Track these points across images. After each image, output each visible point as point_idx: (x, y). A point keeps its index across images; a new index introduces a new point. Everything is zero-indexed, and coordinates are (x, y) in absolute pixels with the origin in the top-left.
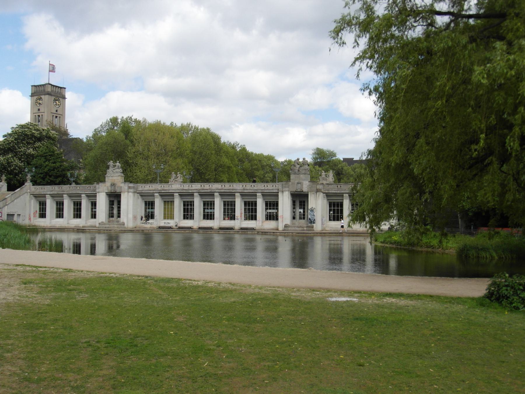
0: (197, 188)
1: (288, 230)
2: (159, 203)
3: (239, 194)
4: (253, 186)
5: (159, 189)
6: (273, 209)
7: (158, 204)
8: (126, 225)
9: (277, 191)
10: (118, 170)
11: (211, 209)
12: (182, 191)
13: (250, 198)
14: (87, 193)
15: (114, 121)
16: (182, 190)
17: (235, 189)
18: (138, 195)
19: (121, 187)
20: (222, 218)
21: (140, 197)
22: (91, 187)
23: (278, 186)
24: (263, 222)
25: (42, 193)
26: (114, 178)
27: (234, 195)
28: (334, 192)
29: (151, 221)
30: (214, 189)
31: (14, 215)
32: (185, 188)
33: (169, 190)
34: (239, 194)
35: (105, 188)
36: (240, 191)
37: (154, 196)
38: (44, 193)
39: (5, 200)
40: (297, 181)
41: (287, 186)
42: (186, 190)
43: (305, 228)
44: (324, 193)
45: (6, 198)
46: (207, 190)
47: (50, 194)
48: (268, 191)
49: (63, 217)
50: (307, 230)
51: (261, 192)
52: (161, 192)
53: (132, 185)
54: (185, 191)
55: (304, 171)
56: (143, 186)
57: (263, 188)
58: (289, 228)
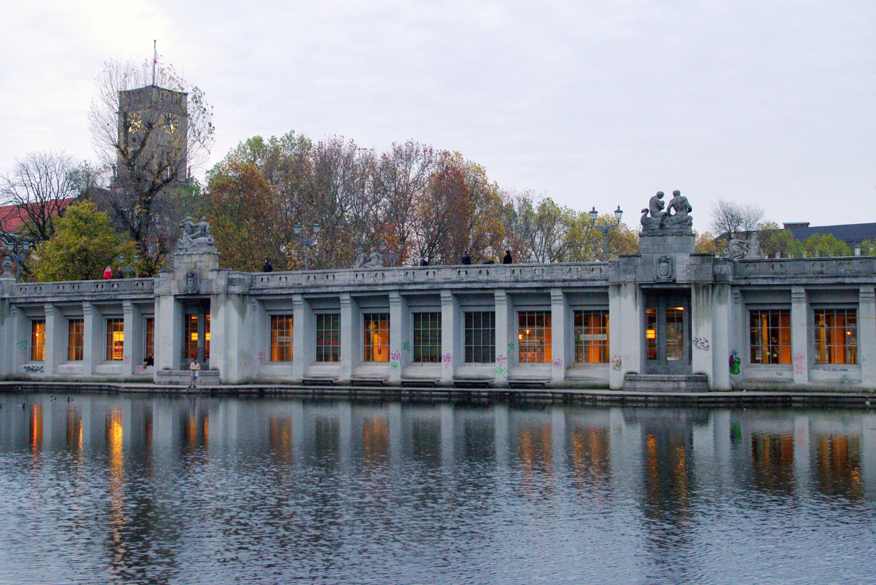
0: (396, 280)
1: (635, 389)
2: (301, 319)
3: (502, 293)
4: (265, 280)
5: (304, 284)
6: (596, 332)
8: (222, 376)
9: (604, 283)
12: (359, 289)
13: (533, 303)
14: (135, 297)
15: (256, 143)
16: (360, 285)
17: (491, 282)
18: (254, 300)
19: (211, 281)
20: (362, 357)
21: (257, 304)
22: (145, 283)
23: (607, 271)
24: (568, 368)
25: (36, 300)
26: (195, 258)
27: (492, 296)
28: (765, 282)
30: (439, 280)
32: (366, 281)
33: (328, 286)
34: (502, 293)
35: (174, 284)
36: (508, 285)
37: (290, 301)
38: (40, 300)
40: (657, 257)
41: (631, 268)
42: (368, 285)
43: (683, 385)
44: (733, 286)
46: (423, 283)
47: (53, 302)
48: (579, 284)
49: (82, 359)
50: (686, 390)
52: (307, 291)
54: (365, 288)
55: (677, 226)
56: (265, 278)
57: (568, 277)
58: (638, 385)
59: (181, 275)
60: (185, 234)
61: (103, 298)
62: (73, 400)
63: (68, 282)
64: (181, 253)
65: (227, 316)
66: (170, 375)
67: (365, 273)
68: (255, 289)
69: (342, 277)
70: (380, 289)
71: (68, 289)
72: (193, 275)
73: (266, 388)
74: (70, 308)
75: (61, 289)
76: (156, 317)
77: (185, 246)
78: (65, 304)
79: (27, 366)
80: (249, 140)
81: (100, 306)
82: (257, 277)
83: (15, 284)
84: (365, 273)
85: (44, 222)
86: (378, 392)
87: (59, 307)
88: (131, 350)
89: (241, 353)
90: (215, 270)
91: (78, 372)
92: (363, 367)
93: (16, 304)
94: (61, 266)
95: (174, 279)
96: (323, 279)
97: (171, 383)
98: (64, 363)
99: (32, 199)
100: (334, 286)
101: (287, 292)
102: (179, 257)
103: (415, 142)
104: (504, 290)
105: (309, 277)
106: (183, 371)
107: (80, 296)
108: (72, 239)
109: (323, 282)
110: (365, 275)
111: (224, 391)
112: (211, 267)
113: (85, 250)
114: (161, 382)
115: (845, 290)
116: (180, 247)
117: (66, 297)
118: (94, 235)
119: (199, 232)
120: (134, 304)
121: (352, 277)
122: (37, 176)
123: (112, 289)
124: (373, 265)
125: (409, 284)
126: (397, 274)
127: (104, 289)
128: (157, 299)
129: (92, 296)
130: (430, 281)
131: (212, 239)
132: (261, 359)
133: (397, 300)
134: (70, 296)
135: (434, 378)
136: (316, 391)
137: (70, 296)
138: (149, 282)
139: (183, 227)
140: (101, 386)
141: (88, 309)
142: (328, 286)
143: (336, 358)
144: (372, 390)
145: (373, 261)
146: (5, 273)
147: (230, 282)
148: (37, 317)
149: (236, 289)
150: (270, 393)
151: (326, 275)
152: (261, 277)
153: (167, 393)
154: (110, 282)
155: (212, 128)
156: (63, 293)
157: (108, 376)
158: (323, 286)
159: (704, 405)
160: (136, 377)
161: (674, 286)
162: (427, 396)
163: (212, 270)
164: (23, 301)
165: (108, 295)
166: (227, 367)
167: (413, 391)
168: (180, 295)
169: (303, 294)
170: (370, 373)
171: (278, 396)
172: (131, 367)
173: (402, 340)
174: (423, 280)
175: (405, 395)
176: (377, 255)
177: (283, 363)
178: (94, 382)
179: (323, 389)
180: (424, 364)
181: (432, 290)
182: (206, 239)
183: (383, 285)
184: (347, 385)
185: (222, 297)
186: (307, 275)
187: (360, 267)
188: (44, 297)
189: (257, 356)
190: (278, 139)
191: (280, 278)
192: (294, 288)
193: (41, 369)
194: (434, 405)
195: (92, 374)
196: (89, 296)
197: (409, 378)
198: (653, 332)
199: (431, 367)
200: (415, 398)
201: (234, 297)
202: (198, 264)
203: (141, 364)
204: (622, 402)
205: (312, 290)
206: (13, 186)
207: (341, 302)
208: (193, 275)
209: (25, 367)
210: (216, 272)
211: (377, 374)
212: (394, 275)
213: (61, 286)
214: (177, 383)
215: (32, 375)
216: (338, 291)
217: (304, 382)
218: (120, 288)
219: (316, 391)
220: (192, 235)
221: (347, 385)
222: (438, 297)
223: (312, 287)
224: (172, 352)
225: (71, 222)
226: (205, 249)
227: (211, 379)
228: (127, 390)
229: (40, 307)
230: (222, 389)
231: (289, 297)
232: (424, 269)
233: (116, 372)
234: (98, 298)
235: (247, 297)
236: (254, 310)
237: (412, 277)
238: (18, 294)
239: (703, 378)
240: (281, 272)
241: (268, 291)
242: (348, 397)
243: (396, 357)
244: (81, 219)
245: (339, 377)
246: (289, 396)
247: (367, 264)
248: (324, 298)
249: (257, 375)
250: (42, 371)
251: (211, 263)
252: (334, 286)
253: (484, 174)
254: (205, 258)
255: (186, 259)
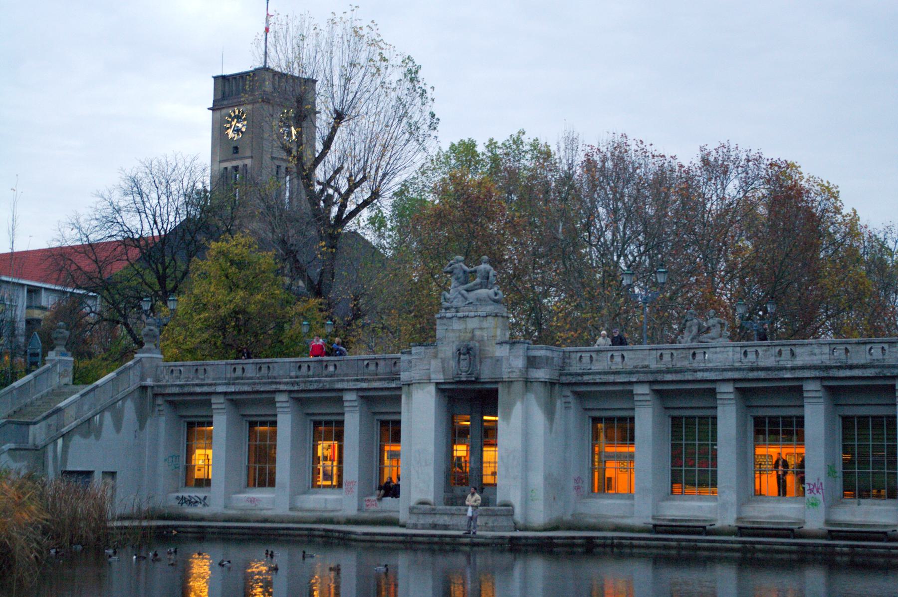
0: (816, 360)
5: (654, 366)
7: (649, 431)
10: (483, 292)
11: (873, 438)
12: (752, 375)
14: (365, 385)
16: (752, 369)
18: (567, 392)
19: (498, 360)
21: (571, 399)
22: (381, 363)
25: (198, 390)
26: (472, 324)
29: (388, 499)
31: (89, 474)
32: (762, 364)
33: (695, 371)
35: (435, 364)
38: (205, 389)
39: (55, 417)
45: (60, 410)
46: (864, 367)
47: (225, 393)
51: (651, 383)
52: (660, 377)
53: (802, 351)
54: (762, 375)
59: (447, 350)
60: (454, 283)
61: (311, 388)
62: (312, 557)
63: (251, 361)
64: (449, 315)
65: (527, 418)
66: (433, 512)
67: (760, 350)
68: (570, 374)
69: (719, 356)
70: (788, 375)
71: (251, 371)
72: (469, 350)
73: (598, 538)
74: (254, 403)
75: (239, 372)
76: (404, 419)
77: (455, 303)
78: (244, 397)
79: (180, 495)
80: (453, 145)
81: (372, 397)
82: (573, 355)
83: (162, 364)
84: (760, 350)
85: (165, 269)
86: (794, 548)
87: (235, 401)
88: (357, 473)
89: (548, 478)
90: (506, 343)
91: (265, 506)
92: (755, 505)
93: (163, 395)
94: (206, 335)
95: (436, 357)
96: (686, 358)
97: (435, 526)
98: (240, 492)
99: (147, 232)
100: (707, 370)
101: (626, 380)
102: (445, 321)
103: (733, 147)
104: (287, 393)
105: (661, 355)
106: (448, 507)
107: (272, 383)
108: (222, 295)
109: (686, 364)
110: (761, 353)
111: (530, 541)
112: (499, 338)
113: (244, 312)
114: (419, 526)
115: (327, 398)
116: (446, 304)
117: (249, 384)
118: (251, 288)
119: (478, 280)
120: (362, 397)
121: (738, 356)
122: (154, 195)
123: (325, 372)
124: (713, 339)
125: (839, 368)
126: (817, 351)
127: (311, 373)
128: (405, 389)
129: (293, 384)
130: (877, 363)
131: (500, 292)
132: (578, 488)
133: (818, 394)
134: (254, 384)
135: (885, 526)
136: (684, 543)
137: (254, 384)
138: (388, 362)
139: (451, 272)
140: (311, 529)
141: (285, 405)
142: (695, 371)
143: (272, 483)
144: (783, 544)
145: (714, 333)
146: (146, 346)
147: (532, 362)
148: (196, 416)
149: (541, 374)
150: (604, 546)
151: (692, 351)
152: (579, 354)
153: (436, 543)
154: (322, 361)
155: (435, 121)
156: (242, 379)
157: (319, 514)
158: (688, 370)
159: (643, 551)
160: (365, 515)
161: (479, 386)
162: (883, 556)
163: (501, 343)
164: (176, 390)
165: (320, 381)
166: (526, 502)
167: (858, 546)
168: (444, 383)
169: (651, 383)
170: (768, 514)
171: (615, 550)
172: (356, 499)
173: (826, 461)
174: (863, 362)
175: (842, 554)
176: (719, 323)
177: (201, 489)
178: (258, 521)
179: (695, 541)
180: (862, 501)
181: (881, 378)
182: (491, 292)
183: (793, 369)
184: (730, 533)
185: (518, 387)
186: (659, 352)
187: (692, 340)
188: (211, 385)
189: (572, 484)
190: (499, 144)
191: (612, 356)
192: (638, 372)
193: (204, 501)
194: (705, 565)
195: (291, 509)
196: (287, 383)
197: (839, 525)
198: (464, 447)
199: (875, 507)
200: (859, 560)
201: (540, 389)
202: (477, 333)
203: (372, 494)
204: (409, 544)
205: (669, 377)
206: (118, 211)
207: (718, 396)
208: (469, 350)
209: (177, 498)
210: (508, 346)
211: (782, 517)
212: (813, 354)
213: (239, 368)
214: (446, 527)
215: (190, 510)
216: (714, 378)
217: (656, 529)
218: (338, 371)
219: (684, 543)
220: (465, 286)
221: (730, 533)
222: (798, 391)
223: (668, 371)
224: (432, 475)
225: (218, 267)
226: (490, 308)
227: (503, 521)
228: (368, 538)
229: (205, 401)
230: (526, 538)
231: (628, 388)
232: (865, 343)
233: (330, 506)
234: (302, 387)
235: (557, 386)
236: (566, 408)
237: (843, 357)
238: (167, 379)
239: (509, 511)
240: (583, 348)
241: (591, 377)
242: (427, 547)
243: (815, 489)
244: (232, 262)
245: (716, 520)
246: (635, 550)
247: (704, 337)
248: (672, 390)
249: (572, 515)
250: (205, 505)
251: (499, 332)
252: (707, 370)
253: (836, 198)
254: (490, 322)
255: (457, 325)
